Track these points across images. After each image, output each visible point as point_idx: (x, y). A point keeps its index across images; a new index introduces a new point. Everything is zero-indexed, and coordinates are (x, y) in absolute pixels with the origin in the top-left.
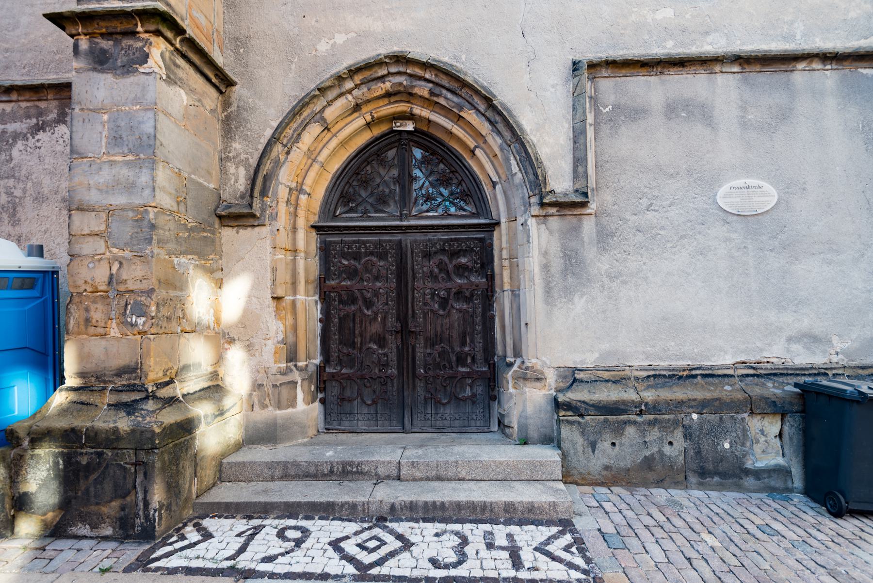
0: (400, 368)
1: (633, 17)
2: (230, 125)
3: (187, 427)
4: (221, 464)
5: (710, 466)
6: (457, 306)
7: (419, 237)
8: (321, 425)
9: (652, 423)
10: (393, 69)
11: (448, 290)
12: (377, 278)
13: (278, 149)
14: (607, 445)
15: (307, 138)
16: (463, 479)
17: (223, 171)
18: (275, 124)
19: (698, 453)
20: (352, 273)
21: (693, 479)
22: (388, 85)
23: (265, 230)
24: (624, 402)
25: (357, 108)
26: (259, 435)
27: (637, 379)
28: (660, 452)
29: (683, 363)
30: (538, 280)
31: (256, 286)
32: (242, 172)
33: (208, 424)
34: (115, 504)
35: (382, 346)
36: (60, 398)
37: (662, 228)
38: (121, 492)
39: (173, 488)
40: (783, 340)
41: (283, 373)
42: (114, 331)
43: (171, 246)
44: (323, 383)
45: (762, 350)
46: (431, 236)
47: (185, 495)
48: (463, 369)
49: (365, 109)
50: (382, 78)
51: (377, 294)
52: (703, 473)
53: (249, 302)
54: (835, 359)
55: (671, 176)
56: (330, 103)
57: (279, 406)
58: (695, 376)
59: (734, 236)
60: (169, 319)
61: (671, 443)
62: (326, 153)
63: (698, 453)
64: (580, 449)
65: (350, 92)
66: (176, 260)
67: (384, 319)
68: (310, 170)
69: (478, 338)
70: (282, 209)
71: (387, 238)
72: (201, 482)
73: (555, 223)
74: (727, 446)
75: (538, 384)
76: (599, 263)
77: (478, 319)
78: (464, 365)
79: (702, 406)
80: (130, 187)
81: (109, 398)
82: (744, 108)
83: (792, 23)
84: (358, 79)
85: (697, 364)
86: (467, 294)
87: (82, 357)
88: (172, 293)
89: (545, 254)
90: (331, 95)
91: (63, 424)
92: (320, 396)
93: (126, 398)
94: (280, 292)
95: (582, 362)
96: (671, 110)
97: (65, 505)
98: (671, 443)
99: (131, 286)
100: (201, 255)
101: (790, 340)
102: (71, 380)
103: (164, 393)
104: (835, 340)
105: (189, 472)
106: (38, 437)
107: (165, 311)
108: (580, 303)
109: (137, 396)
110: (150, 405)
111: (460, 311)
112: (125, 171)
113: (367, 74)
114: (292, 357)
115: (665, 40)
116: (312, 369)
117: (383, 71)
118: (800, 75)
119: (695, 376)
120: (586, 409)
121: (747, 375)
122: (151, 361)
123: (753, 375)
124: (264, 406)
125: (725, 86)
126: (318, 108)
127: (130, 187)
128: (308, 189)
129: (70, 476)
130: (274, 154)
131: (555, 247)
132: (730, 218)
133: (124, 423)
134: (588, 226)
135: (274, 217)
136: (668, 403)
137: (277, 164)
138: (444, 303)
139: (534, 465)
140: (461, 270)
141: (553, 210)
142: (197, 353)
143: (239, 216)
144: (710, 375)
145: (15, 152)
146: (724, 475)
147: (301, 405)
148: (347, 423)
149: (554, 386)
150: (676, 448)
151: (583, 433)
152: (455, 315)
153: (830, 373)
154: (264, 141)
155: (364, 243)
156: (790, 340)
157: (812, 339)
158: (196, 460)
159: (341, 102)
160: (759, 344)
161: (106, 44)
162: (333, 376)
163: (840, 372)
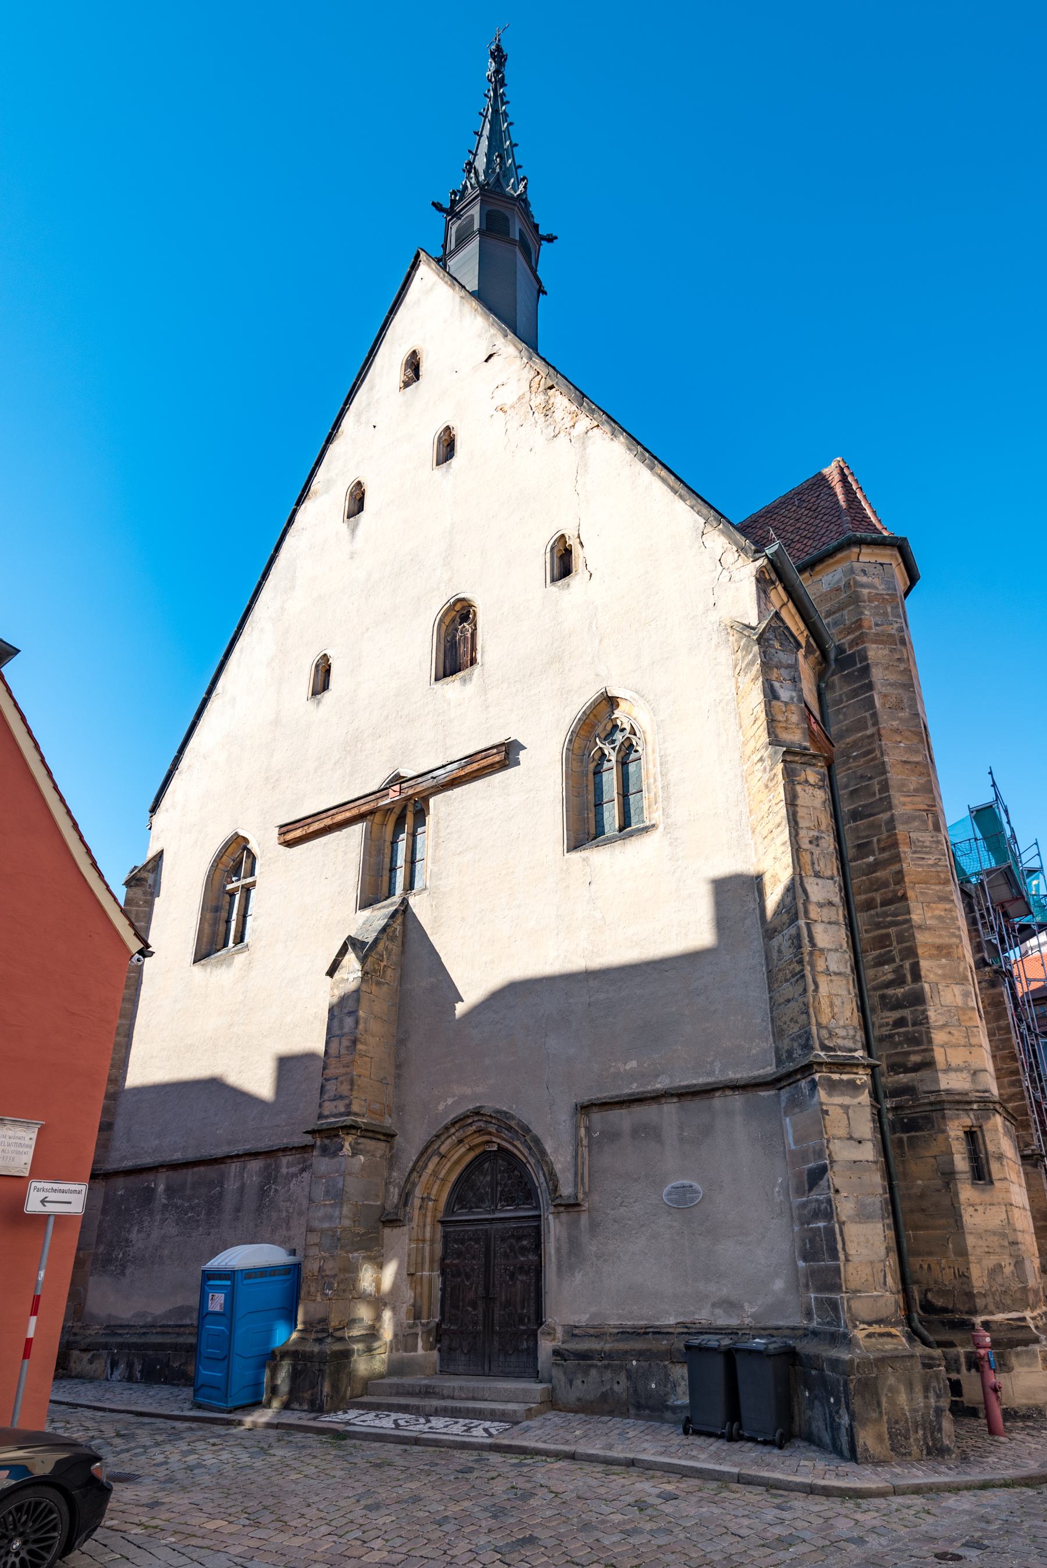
0: (484, 1326)
1: (612, 1070)
2: (392, 1161)
3: (347, 1354)
4: (367, 1384)
5: (643, 1401)
6: (520, 1277)
7: (500, 1226)
8: (438, 1368)
9: (606, 1367)
10: (476, 1119)
11: (515, 1266)
12: (474, 1258)
13: (415, 1174)
14: (579, 1382)
15: (431, 1166)
16: (486, 1400)
17: (387, 1190)
18: (414, 1158)
19: (635, 1391)
20: (459, 1254)
21: (632, 1411)
22: (474, 1127)
23: (405, 1229)
24: (591, 1351)
25: (460, 1141)
26: (396, 1368)
27: (611, 1334)
28: (611, 1388)
29: (642, 1323)
30: (554, 1259)
31: (399, 1268)
32: (397, 1190)
33: (359, 1355)
34: (310, 1392)
35: (475, 1309)
36: (295, 1335)
37: (630, 1219)
38: (313, 1386)
39: (335, 1387)
40: (709, 1305)
41: (411, 1327)
42: (319, 1299)
43: (348, 1248)
44: (439, 1336)
45: (694, 1313)
46: (506, 1225)
47: (342, 1394)
48: (522, 1327)
49: (466, 1141)
50: (470, 1124)
51: (473, 1270)
52: (639, 1407)
53: (396, 1278)
54: (747, 1321)
55: (636, 1180)
56: (443, 1143)
57: (406, 1351)
58: (647, 1333)
59: (675, 1224)
60: (344, 1291)
61: (618, 1383)
62: (444, 1172)
63: (635, 1391)
64: (563, 1385)
65: (454, 1134)
66: (351, 1255)
67: (477, 1288)
68: (436, 1186)
69: (532, 1302)
70: (416, 1212)
71: (481, 1227)
72: (352, 1390)
73: (564, 1217)
74: (653, 1386)
75: (548, 1337)
76: (592, 1247)
77: (532, 1288)
78: (523, 1325)
79: (640, 1355)
80: (330, 1218)
81: (313, 1336)
82: (681, 1128)
83: (713, 1062)
84: (457, 1126)
85: (651, 1323)
86: (526, 1267)
87: (306, 1313)
88: (347, 1275)
89: (558, 1240)
90: (443, 1138)
91: (293, 1348)
92: (438, 1346)
93: (320, 1335)
94: (412, 1271)
95: (579, 1321)
96: (635, 1132)
97: (291, 1392)
98: (618, 1383)
99: (328, 1273)
100: (367, 1249)
101: (714, 1305)
102: (300, 1327)
103: (338, 1334)
104: (746, 1305)
105: (345, 1381)
106: (284, 1354)
107: (342, 1287)
108: (578, 1277)
109: (325, 1335)
110: (329, 1340)
111: (522, 1282)
112: (329, 1210)
113: (462, 1123)
114: (417, 1316)
115: (632, 1083)
116: (433, 1325)
117: (470, 1121)
118: (718, 1101)
119: (647, 1333)
120: (575, 1359)
121: (682, 1333)
122: (332, 1316)
123: (686, 1333)
124: (398, 1350)
125: (670, 1109)
126: (436, 1147)
127: (330, 1218)
128: (433, 1197)
129: (295, 1376)
130: (412, 1179)
131: (564, 1235)
132: (672, 1211)
133: (316, 1349)
134: (584, 1218)
135: (411, 1220)
136: (617, 1351)
137: (414, 1185)
138: (512, 1276)
139: (525, 1391)
140: (524, 1250)
141: (562, 1209)
142: (364, 1313)
143: (393, 1221)
144: (659, 1332)
145: (292, 1185)
146: (652, 1409)
147: (420, 1351)
148: (452, 1367)
149: (561, 1339)
150: (621, 1387)
151: (565, 1373)
152: (519, 1285)
153: (740, 1333)
154: (408, 1170)
155: (467, 1231)
156: (714, 1305)
157: (730, 1305)
158: (351, 1375)
159: (449, 1141)
160: (692, 1308)
161: (327, 1141)
162: (445, 1330)
163: (747, 1332)
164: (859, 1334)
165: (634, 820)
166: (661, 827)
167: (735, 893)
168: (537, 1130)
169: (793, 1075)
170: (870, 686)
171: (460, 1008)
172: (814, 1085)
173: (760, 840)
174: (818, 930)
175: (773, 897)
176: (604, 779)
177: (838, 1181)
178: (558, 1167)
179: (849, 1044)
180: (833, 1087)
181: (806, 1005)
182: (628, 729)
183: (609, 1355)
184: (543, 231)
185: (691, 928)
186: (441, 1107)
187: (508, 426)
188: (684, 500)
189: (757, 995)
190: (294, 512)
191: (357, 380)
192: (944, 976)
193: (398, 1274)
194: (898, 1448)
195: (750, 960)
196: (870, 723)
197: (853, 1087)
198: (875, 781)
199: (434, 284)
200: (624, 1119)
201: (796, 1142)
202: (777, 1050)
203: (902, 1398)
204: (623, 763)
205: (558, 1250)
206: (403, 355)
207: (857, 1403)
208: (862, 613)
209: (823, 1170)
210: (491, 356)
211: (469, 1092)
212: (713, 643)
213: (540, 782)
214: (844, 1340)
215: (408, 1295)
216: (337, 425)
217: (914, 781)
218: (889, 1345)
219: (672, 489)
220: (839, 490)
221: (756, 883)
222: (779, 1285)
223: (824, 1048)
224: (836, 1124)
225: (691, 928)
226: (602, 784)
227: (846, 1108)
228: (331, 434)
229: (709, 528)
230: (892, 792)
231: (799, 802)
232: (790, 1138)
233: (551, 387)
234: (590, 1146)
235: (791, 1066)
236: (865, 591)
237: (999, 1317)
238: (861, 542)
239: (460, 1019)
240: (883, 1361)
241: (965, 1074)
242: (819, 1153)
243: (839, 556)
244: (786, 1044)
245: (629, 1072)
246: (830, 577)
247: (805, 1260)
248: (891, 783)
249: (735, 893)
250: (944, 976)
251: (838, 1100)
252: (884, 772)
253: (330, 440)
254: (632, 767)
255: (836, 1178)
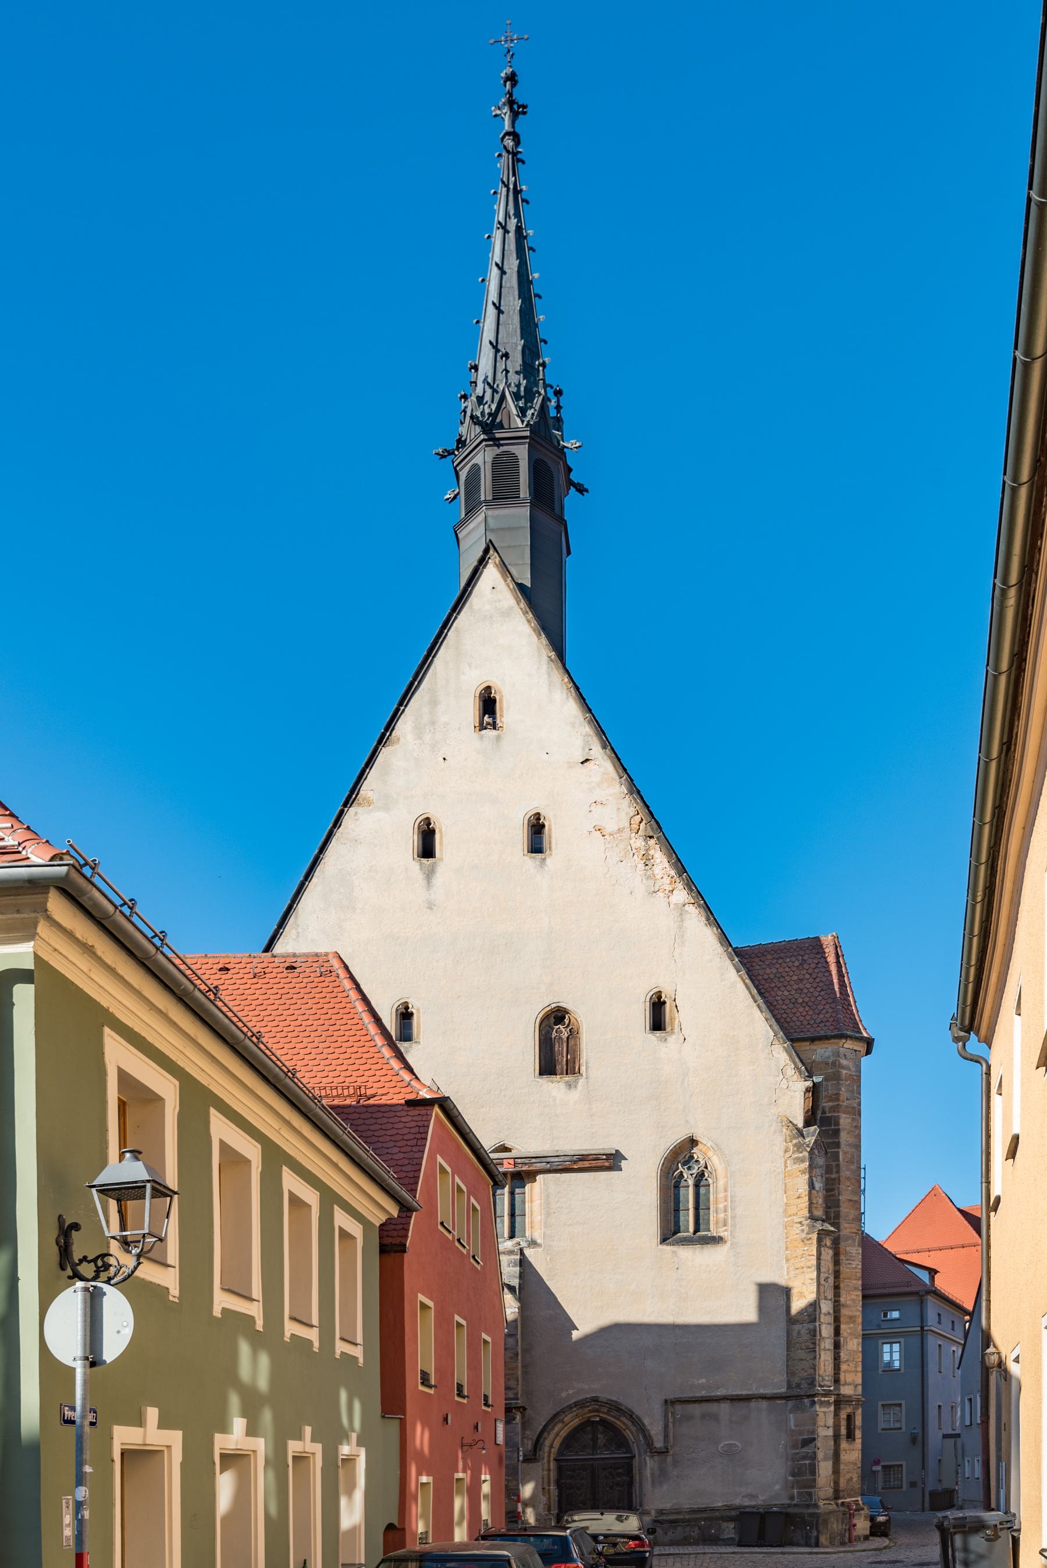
32: (530, 1442)
73: (656, 1458)
79: (705, 1519)
89: (652, 1469)
96: (703, 1416)
108: (665, 1487)
114: (549, 1510)
118: (753, 1404)
125: (724, 1408)
134: (669, 1459)
138: (611, 1488)
144: (713, 1510)
150: (696, 1533)
157: (751, 1496)
164: (821, 1503)
165: (702, 1227)
166: (729, 1244)
167: (772, 1295)
168: (638, 1411)
169: (800, 1394)
170: (838, 1145)
171: (575, 1335)
172: (813, 1403)
173: (791, 1268)
174: (823, 1327)
175: (798, 1304)
176: (681, 1193)
177: (819, 1445)
178: (653, 1433)
179: (829, 1383)
180: (822, 1403)
181: (815, 1366)
182: (702, 1162)
183: (689, 1520)
184: (573, 476)
185: (744, 1310)
186: (564, 1395)
187: (608, 854)
188: (762, 1012)
189: (781, 1352)
190: (341, 813)
191: (415, 679)
192: (851, 1334)
193: (535, 1489)
194: (832, 1544)
195: (778, 1332)
196: (834, 1170)
197: (828, 1403)
198: (832, 1210)
199: (511, 609)
200: (697, 1409)
201: (795, 1426)
202: (789, 1382)
203: (835, 1526)
204: (697, 1186)
205: (652, 1474)
206: (472, 684)
207: (821, 1528)
208: (840, 1089)
209: (814, 1439)
210: (587, 760)
211: (586, 1387)
212: (773, 1129)
213: (638, 1188)
214: (816, 1506)
215: (543, 1499)
216: (390, 726)
217: (853, 1214)
218: (830, 1507)
219: (753, 997)
220: (831, 959)
221: (787, 1292)
222: (777, 1487)
223: (821, 1386)
224: (821, 1421)
225: (744, 1310)
226: (683, 1204)
227: (825, 1413)
228: (383, 735)
229: (776, 1042)
230: (841, 1220)
231: (822, 1257)
232: (792, 1423)
233: (651, 837)
234: (674, 1423)
235: (796, 1392)
236: (844, 1072)
237: (848, 1500)
238: (851, 1037)
239: (576, 1341)
240: (831, 1512)
241: (852, 1387)
242: (813, 1432)
243: (832, 1041)
244: (796, 1380)
245: (700, 1384)
246: (823, 1050)
247: (793, 1476)
248: (841, 1214)
249: (772, 1295)
250: (851, 1334)
251: (823, 1409)
252: (838, 1206)
253: (382, 741)
254: (702, 1190)
255: (819, 1443)
